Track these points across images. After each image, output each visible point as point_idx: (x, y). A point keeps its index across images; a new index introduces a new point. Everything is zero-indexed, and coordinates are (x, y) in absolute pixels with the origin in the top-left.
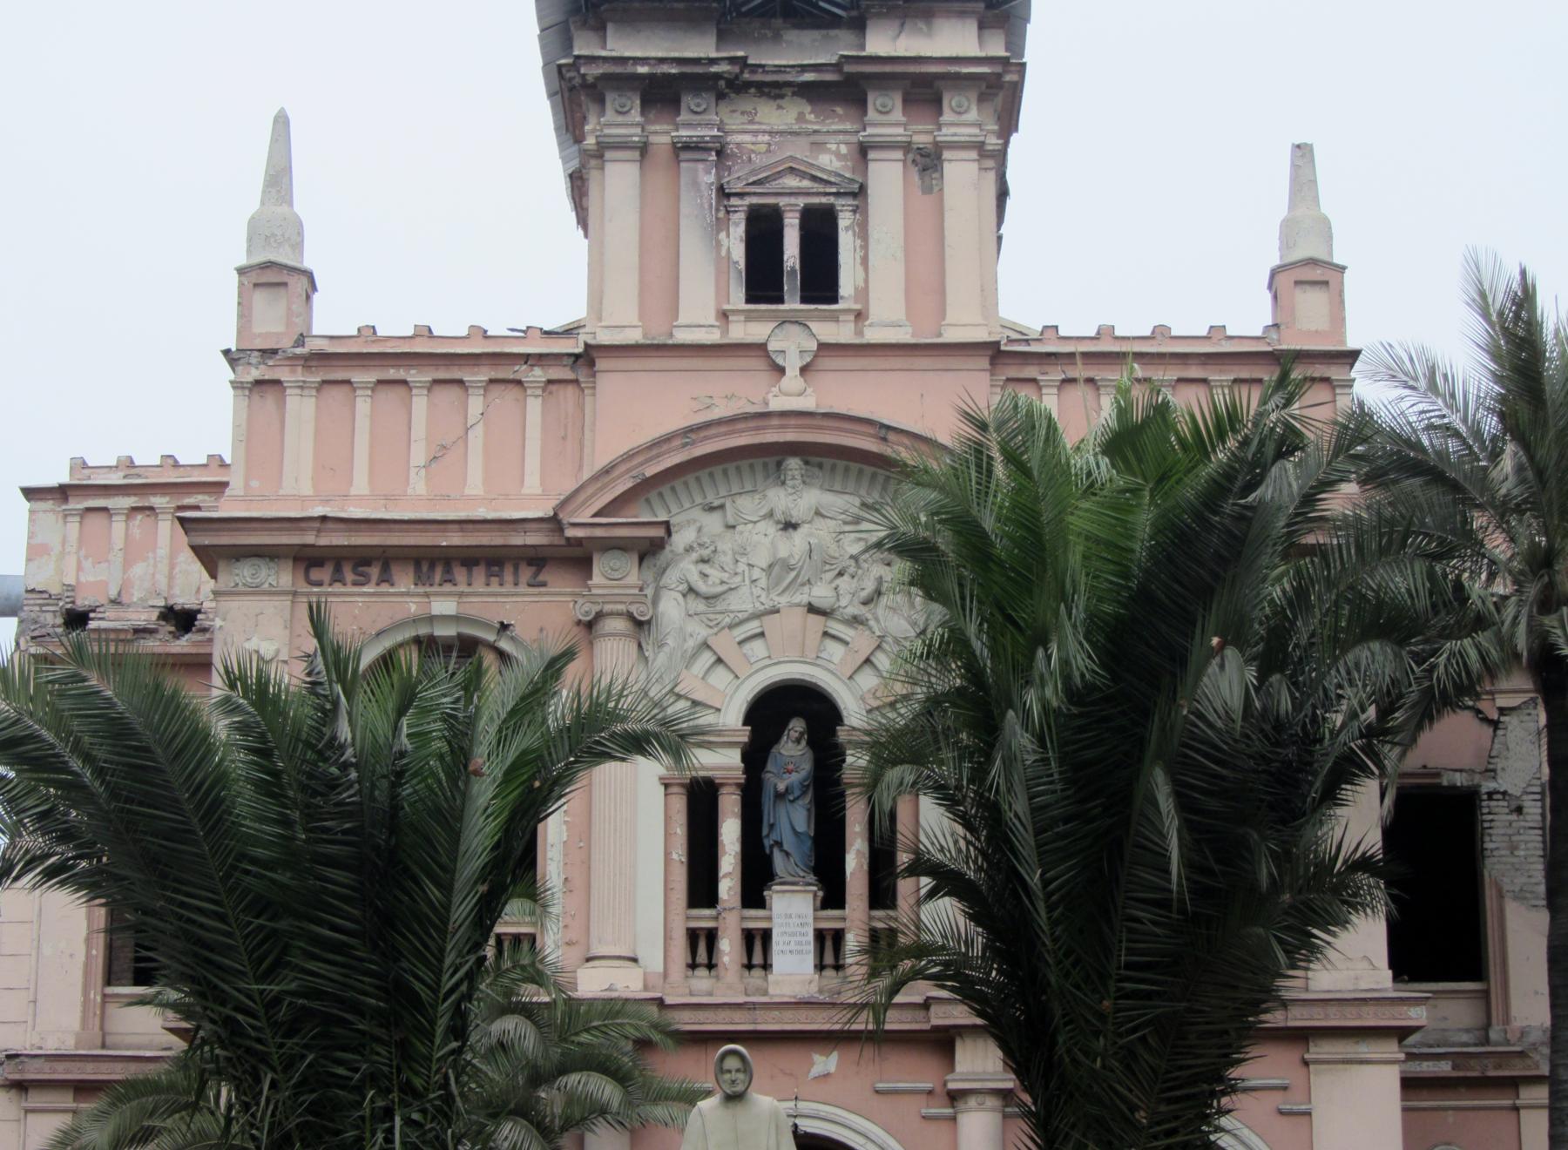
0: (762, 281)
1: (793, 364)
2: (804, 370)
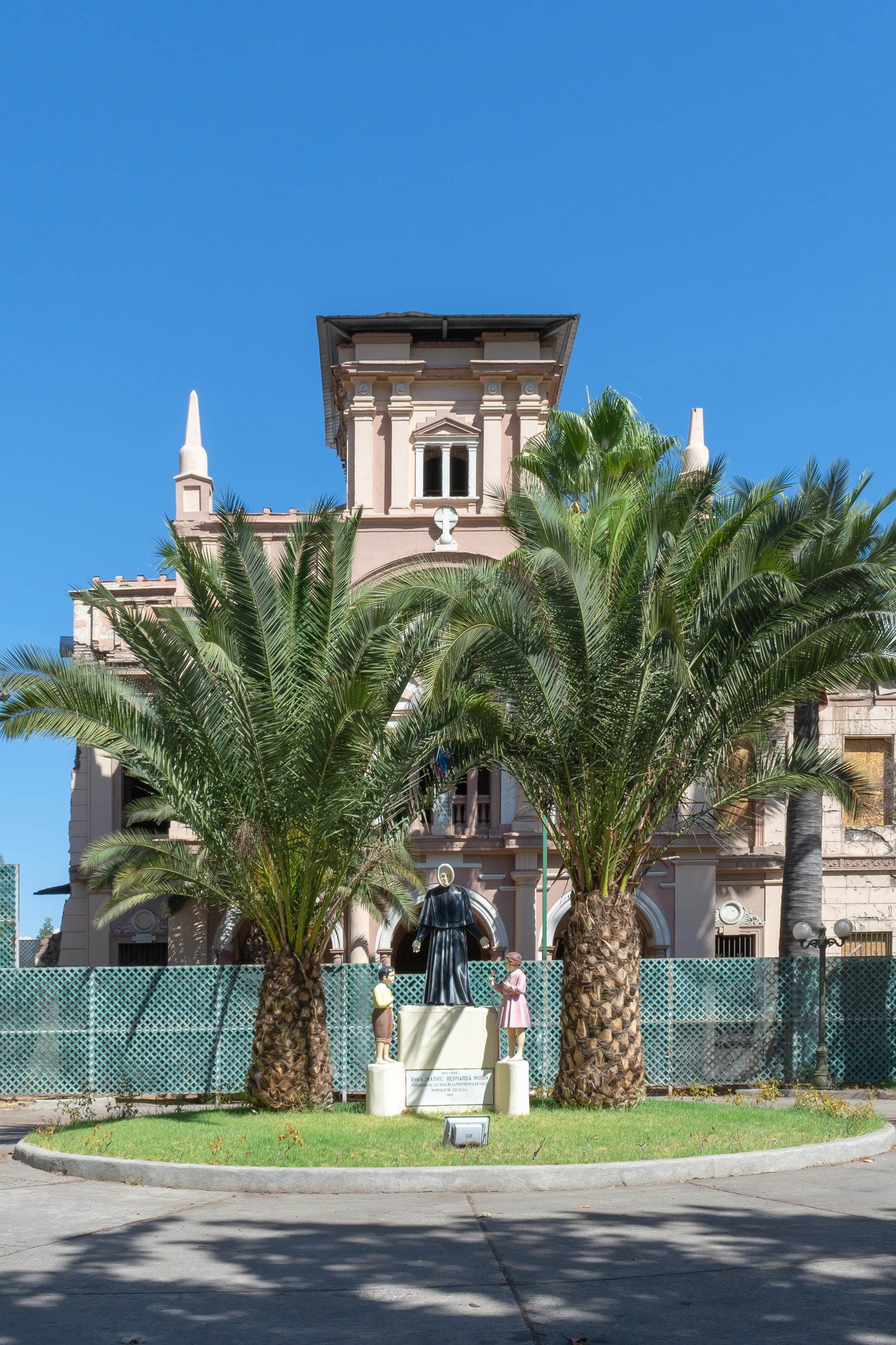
0: (432, 485)
1: (446, 527)
2: (451, 531)
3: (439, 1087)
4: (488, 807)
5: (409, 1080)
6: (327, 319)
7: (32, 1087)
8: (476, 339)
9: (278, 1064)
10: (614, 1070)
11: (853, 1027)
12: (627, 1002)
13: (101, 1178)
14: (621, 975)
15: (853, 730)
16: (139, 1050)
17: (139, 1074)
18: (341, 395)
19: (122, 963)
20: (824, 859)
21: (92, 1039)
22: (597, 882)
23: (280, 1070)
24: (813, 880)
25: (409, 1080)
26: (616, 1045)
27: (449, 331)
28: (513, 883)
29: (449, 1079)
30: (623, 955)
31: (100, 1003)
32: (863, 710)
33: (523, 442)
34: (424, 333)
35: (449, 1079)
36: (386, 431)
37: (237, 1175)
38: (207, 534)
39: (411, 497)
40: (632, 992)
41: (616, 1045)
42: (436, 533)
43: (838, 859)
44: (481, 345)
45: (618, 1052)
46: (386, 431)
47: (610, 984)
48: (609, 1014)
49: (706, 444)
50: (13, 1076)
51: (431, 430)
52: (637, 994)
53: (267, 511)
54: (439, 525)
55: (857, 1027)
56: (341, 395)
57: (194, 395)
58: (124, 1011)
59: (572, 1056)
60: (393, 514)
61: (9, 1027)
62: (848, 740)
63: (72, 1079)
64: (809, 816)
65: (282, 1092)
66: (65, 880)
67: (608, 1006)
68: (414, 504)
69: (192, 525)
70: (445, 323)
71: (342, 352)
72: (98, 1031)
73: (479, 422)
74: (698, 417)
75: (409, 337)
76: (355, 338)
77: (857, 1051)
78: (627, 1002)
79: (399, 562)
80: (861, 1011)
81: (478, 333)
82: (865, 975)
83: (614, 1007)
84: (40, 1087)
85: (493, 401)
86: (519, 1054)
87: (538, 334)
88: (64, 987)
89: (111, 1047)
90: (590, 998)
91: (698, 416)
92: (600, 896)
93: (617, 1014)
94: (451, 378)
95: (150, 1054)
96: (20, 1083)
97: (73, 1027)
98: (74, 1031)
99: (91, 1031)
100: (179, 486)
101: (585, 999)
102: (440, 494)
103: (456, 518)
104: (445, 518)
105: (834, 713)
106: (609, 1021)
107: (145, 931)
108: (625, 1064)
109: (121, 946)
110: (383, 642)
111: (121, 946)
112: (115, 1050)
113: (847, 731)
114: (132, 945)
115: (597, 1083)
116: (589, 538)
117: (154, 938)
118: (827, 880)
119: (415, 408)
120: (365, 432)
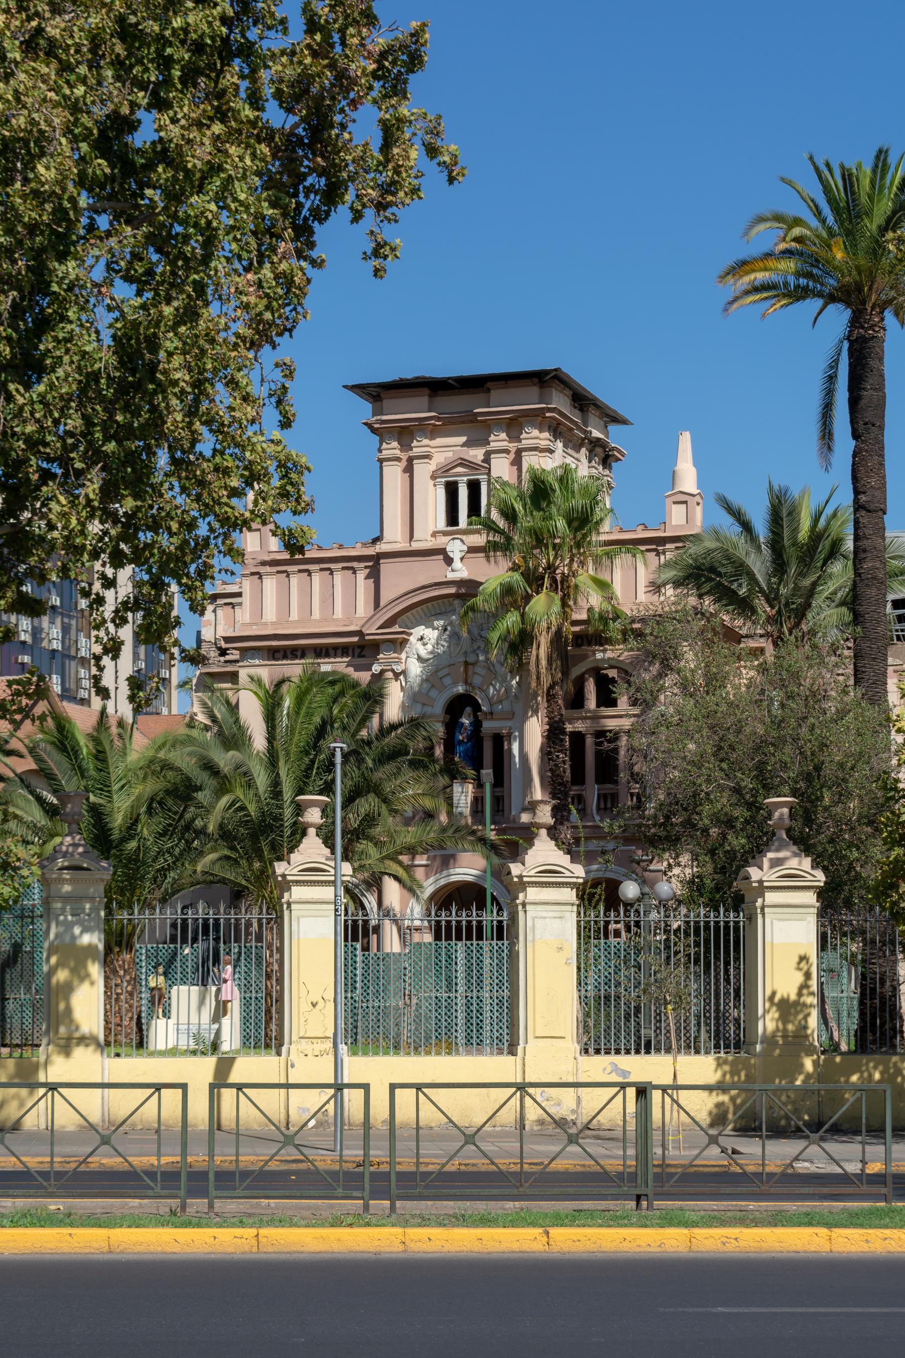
1: (456, 556)
2: (462, 559)
13: (744, 263)
33: (524, 469)
34: (436, 387)
36: (409, 469)
38: (268, 569)
39: (432, 529)
42: (449, 561)
46: (409, 469)
51: (446, 470)
54: (451, 555)
68: (434, 534)
69: (255, 562)
73: (487, 460)
74: (686, 441)
79: (436, 584)
85: (499, 440)
94: (463, 422)
100: (669, 501)
103: (466, 548)
104: (456, 549)
116: (579, 811)
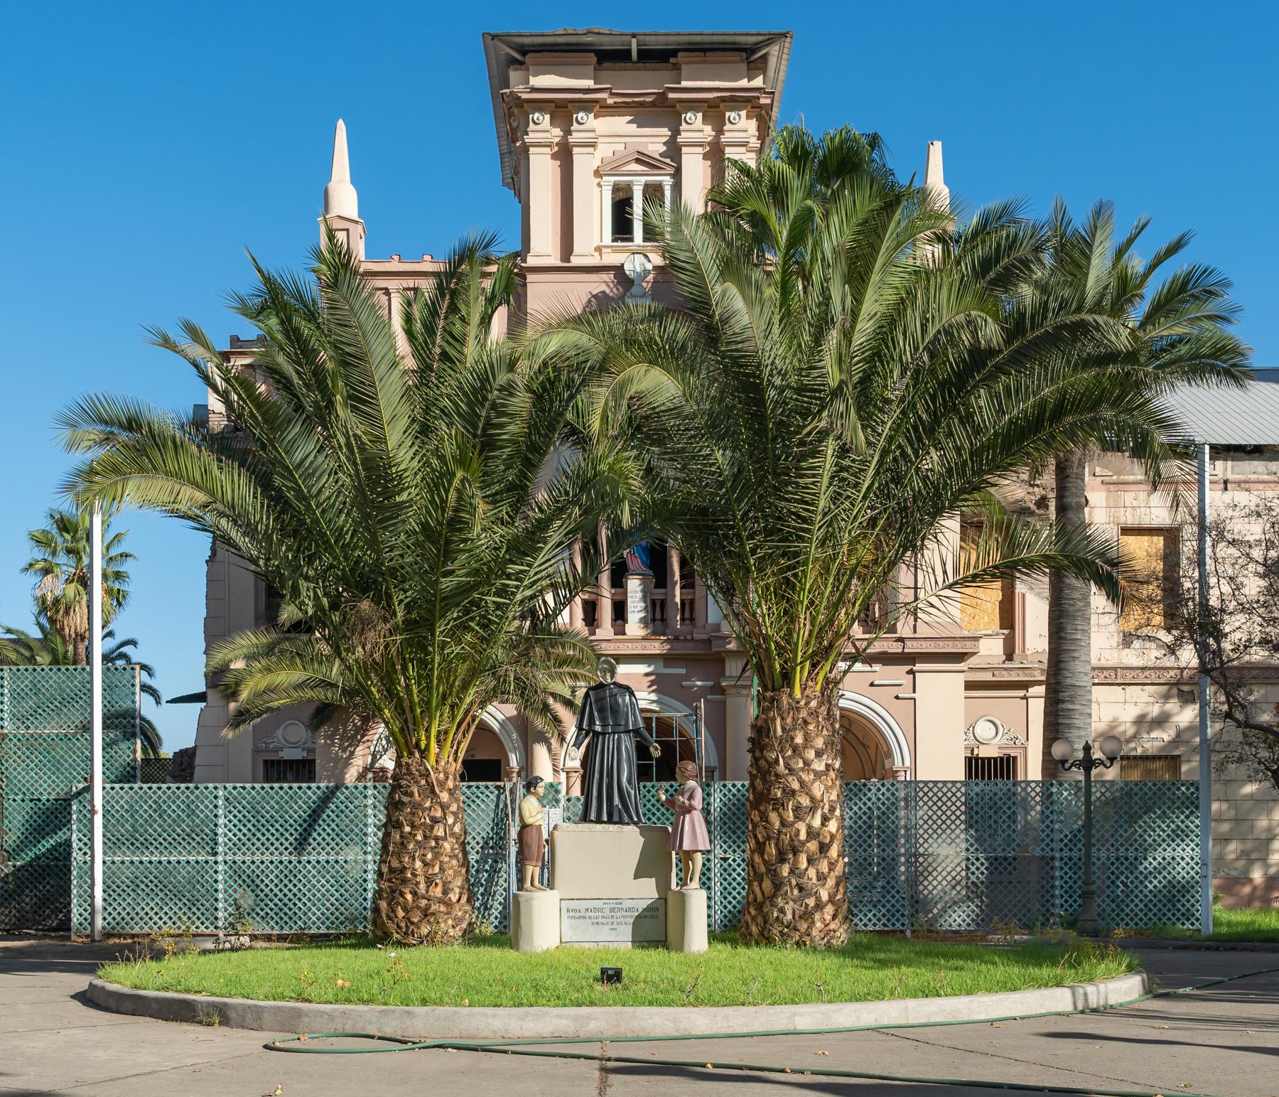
0: (622, 227)
3: (600, 920)
4: (692, 602)
5: (564, 911)
6: (494, 37)
7: (151, 923)
8: (672, 60)
9: (407, 891)
10: (811, 902)
11: (1126, 863)
12: (825, 819)
14: (817, 789)
15: (1131, 519)
16: (276, 881)
17: (276, 909)
18: (515, 124)
19: (267, 779)
20: (1094, 669)
21: (220, 867)
22: (787, 677)
23: (409, 897)
24: (1081, 692)
25: (564, 911)
26: (812, 873)
27: (639, 51)
28: (722, 691)
29: (612, 910)
30: (819, 766)
31: (231, 826)
32: (1143, 495)
35: (612, 910)
37: (330, 1016)
40: (832, 809)
41: (812, 873)
43: (1115, 669)
44: (677, 67)
45: (814, 880)
47: (805, 801)
48: (803, 836)
49: (945, 183)
50: (128, 909)
52: (838, 813)
53: (427, 258)
55: (1131, 863)
56: (515, 124)
57: (341, 125)
58: (259, 835)
59: (760, 885)
60: (575, 261)
61: (124, 853)
62: (1122, 529)
63: (199, 914)
64: (1075, 617)
65: (412, 923)
66: (200, 687)
67: (802, 827)
70: (634, 41)
71: (514, 75)
72: (228, 858)
75: (593, 58)
76: (528, 59)
77: (1132, 892)
78: (825, 819)
80: (1136, 845)
81: (674, 53)
82: (1141, 803)
83: (809, 827)
84: (161, 923)
86: (695, 884)
87: (744, 55)
88: (188, 806)
89: (244, 877)
90: (781, 816)
91: (936, 151)
92: (790, 695)
93: (812, 834)
95: (290, 886)
96: (137, 918)
97: (199, 853)
98: (200, 858)
99: (220, 858)
101: (774, 817)
102: (631, 240)
105: (1107, 498)
106: (803, 843)
107: (294, 745)
108: (825, 896)
109: (266, 762)
110: (511, 395)
111: (266, 762)
112: (248, 881)
113: (1123, 520)
114: (279, 761)
115: (789, 916)
117: (305, 754)
118: (1096, 691)
119: (601, 140)
120: (543, 170)
